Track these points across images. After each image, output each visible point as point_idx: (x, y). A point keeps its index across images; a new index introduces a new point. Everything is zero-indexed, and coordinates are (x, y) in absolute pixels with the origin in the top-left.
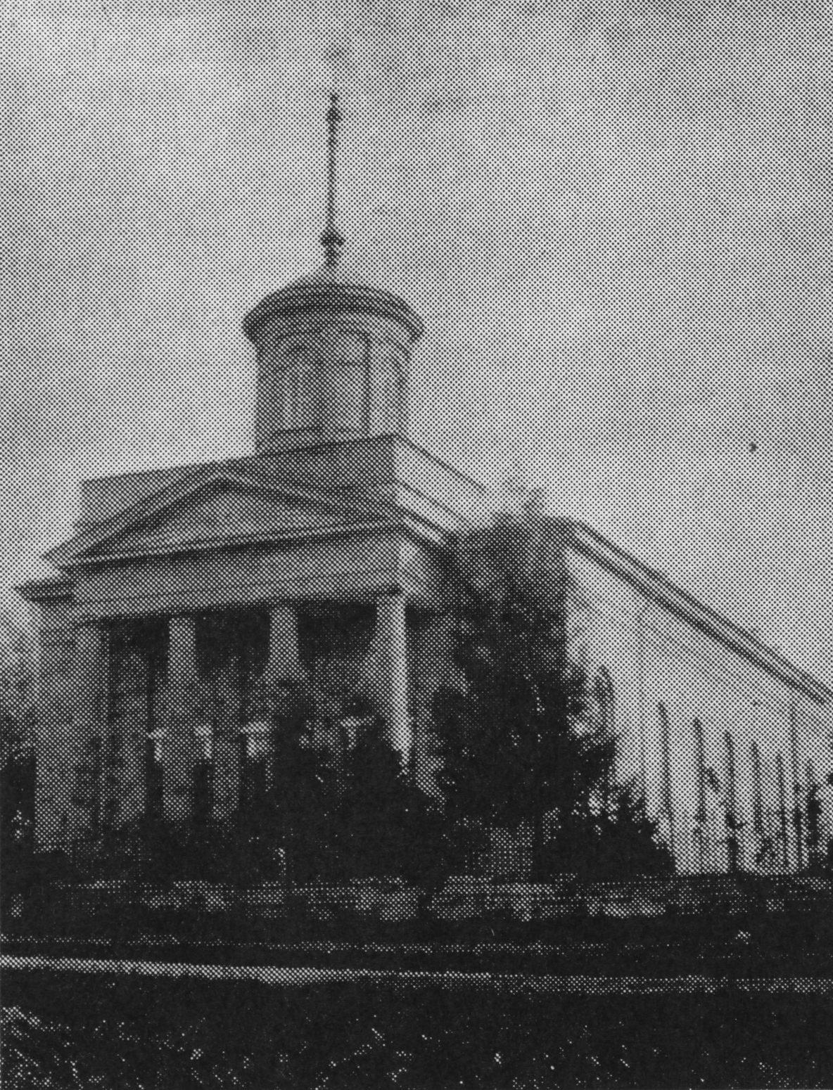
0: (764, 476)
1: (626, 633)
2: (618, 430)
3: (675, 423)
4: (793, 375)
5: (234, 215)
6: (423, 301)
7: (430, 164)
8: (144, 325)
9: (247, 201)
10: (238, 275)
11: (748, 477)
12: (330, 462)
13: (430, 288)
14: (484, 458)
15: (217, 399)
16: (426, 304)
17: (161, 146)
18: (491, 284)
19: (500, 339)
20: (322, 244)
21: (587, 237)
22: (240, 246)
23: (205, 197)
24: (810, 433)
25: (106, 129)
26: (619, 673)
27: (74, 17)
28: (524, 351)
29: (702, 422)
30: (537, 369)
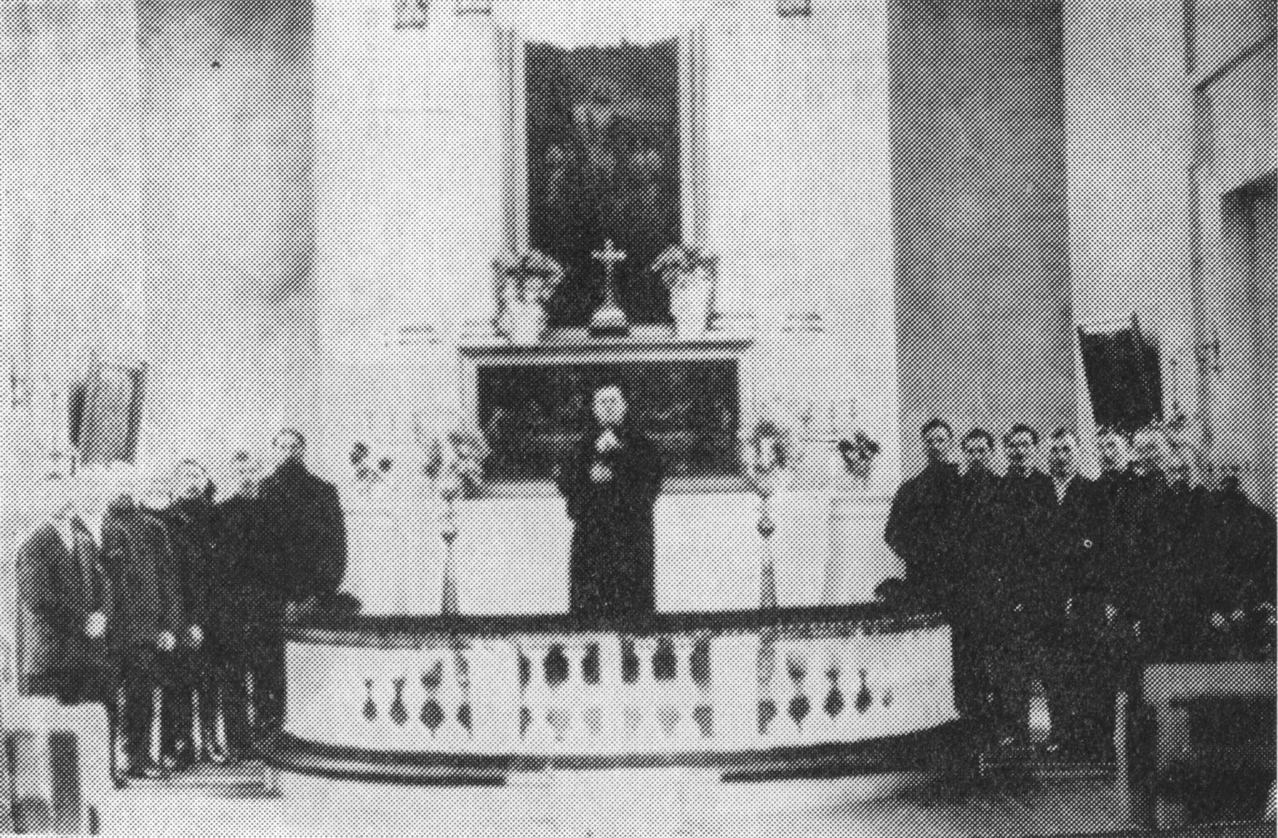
0: (885, 350)
1: (298, 304)
2: (296, 347)
3: (1154, 253)
4: (224, 317)
5: (234, 277)
6: (809, 270)
7: (209, 348)
8: (732, 133)
9: (193, 141)
10: (201, 320)
11: (84, 119)
12: (978, 12)
13: (159, 408)
14: (290, 307)
15: (242, 320)
16: (857, 261)
17: (772, 797)
18: (298, 304)
19: (1090, 155)
20: (1004, 436)
21: (17, 419)
22: (866, 141)
23: (1110, 231)
24: (1151, 54)
25: (85, 164)
26: (717, 103)
27: (311, 322)
28: (809, 547)
29: (39, 326)
30: (260, 438)
